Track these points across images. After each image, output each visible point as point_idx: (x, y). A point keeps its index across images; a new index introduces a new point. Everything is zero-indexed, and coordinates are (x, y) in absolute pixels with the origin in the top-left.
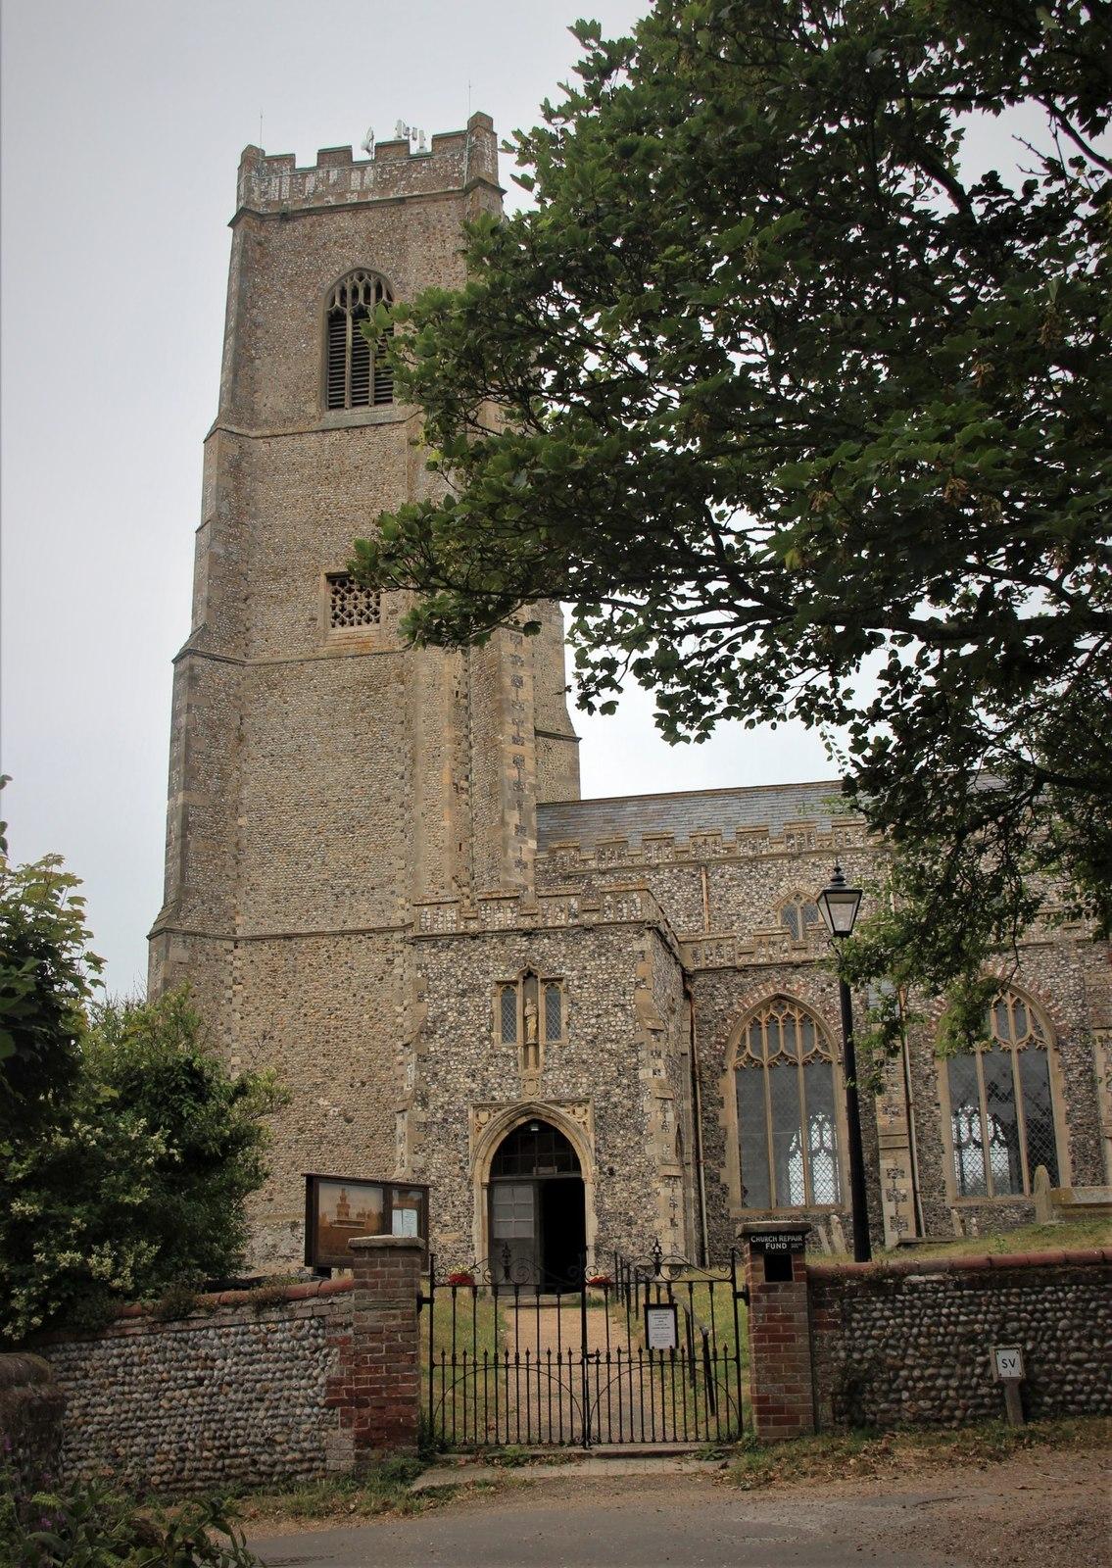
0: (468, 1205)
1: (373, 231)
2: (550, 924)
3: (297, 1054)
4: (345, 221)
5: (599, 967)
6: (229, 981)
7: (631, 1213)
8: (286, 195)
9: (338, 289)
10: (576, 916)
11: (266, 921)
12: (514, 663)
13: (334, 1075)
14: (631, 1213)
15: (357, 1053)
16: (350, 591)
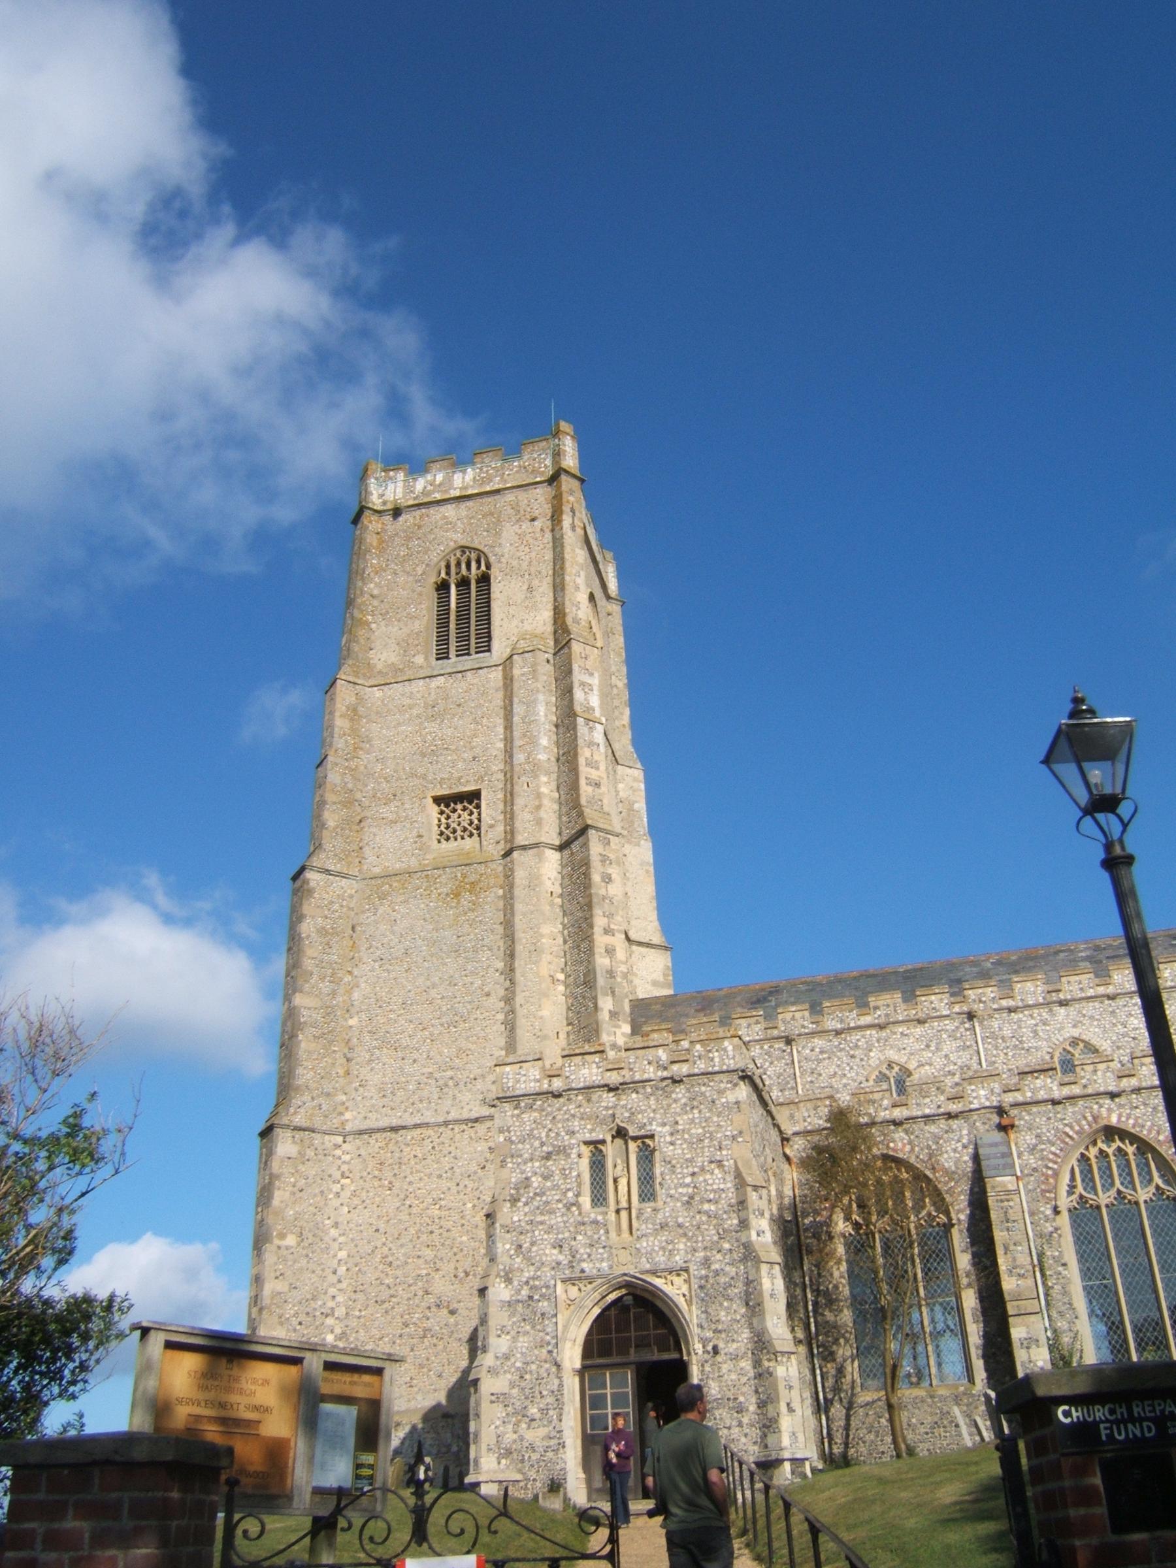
0: (558, 1394)
1: (473, 517)
2: (637, 1077)
3: (402, 1246)
4: (449, 511)
5: (692, 1121)
6: (337, 1175)
7: (742, 1399)
8: (399, 495)
9: (443, 564)
10: (665, 1069)
11: (373, 1116)
12: (603, 862)
13: (438, 1265)
14: (742, 1399)
15: (461, 1243)
16: (454, 811)
